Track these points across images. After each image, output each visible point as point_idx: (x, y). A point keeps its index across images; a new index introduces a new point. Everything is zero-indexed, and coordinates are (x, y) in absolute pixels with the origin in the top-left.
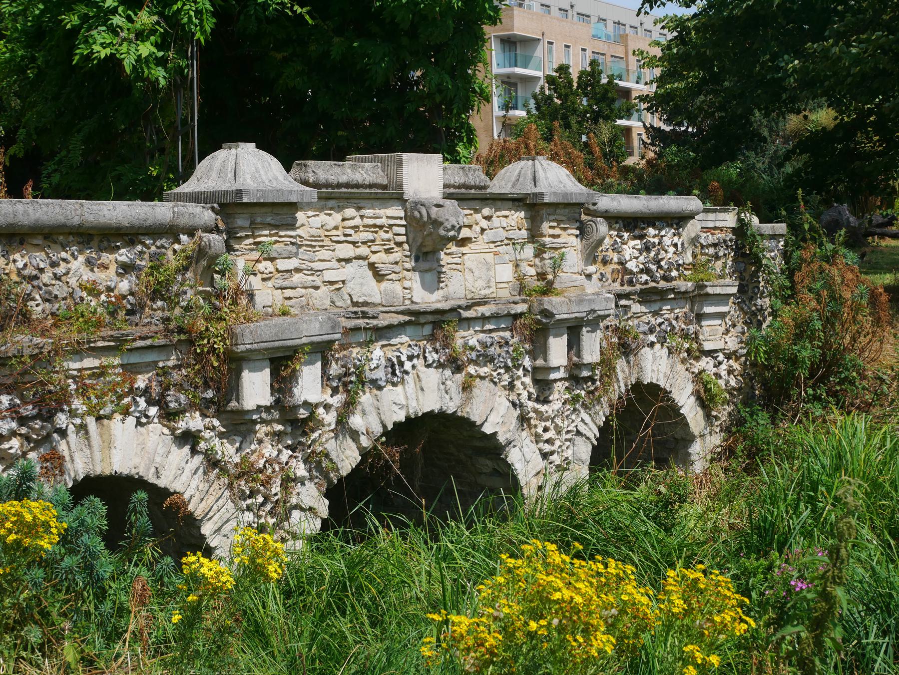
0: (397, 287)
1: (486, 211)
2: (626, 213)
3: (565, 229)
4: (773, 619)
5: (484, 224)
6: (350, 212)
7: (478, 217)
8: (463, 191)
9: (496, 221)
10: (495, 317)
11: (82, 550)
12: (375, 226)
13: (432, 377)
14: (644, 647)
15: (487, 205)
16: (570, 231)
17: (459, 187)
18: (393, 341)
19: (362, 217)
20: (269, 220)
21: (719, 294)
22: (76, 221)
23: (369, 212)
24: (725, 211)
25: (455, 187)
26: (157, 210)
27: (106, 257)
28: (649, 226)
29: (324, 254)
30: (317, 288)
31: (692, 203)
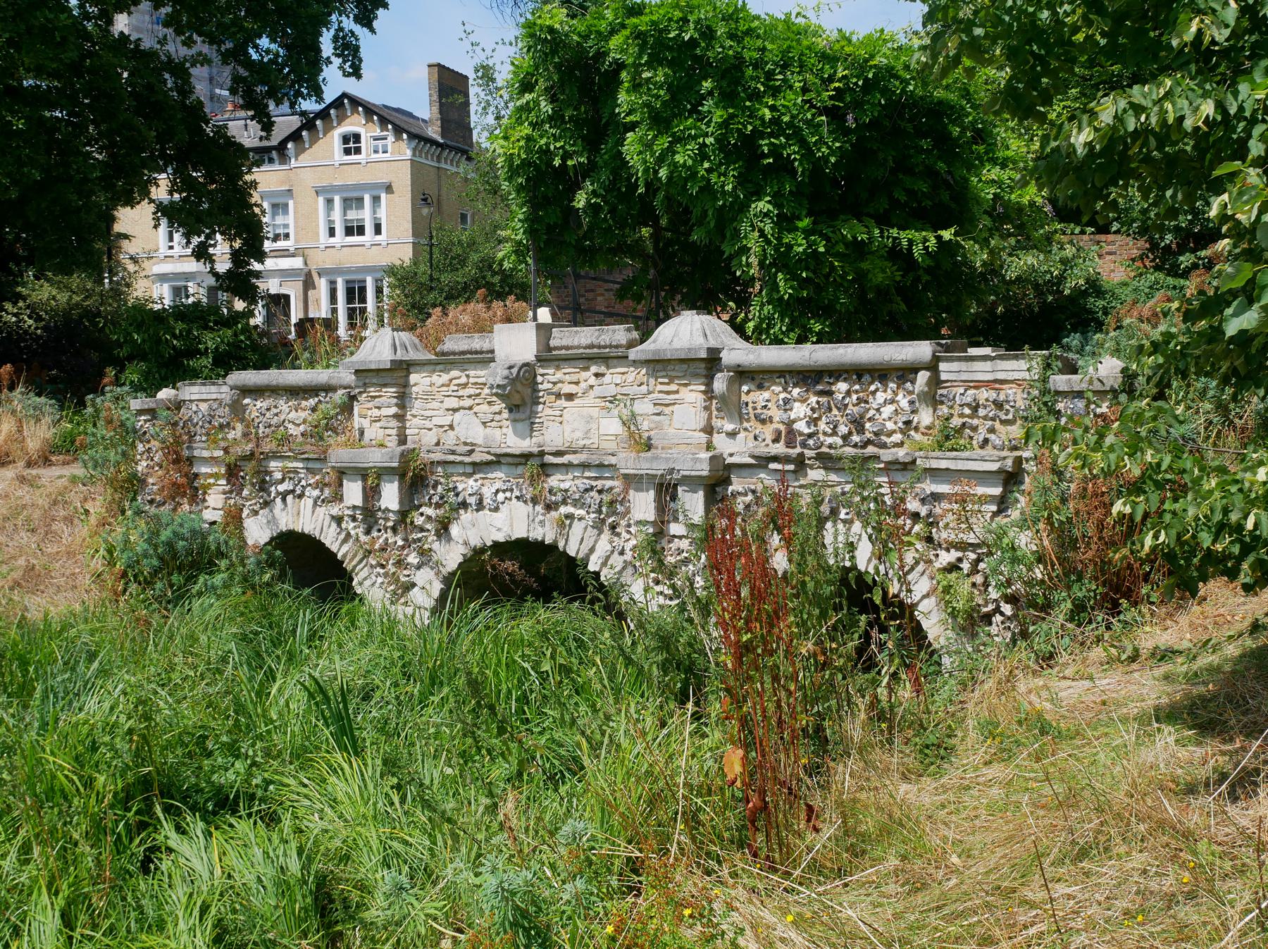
0: (498, 432)
1: (594, 369)
2: (881, 364)
3: (686, 385)
4: (18, 284)
5: (592, 380)
6: (454, 373)
7: (584, 375)
8: (595, 350)
9: (607, 379)
10: (584, 466)
11: (232, 502)
12: (996, 381)
13: (522, 510)
14: (734, 887)
15: (596, 363)
16: (691, 387)
17: (585, 348)
18: (489, 476)
19: (468, 376)
20: (374, 381)
21: (947, 469)
22: (274, 383)
23: (472, 373)
24: (1016, 358)
25: (585, 348)
26: (807, 354)
27: (304, 403)
28: (837, 380)
29: (435, 405)
30: (430, 429)
31: (921, 350)
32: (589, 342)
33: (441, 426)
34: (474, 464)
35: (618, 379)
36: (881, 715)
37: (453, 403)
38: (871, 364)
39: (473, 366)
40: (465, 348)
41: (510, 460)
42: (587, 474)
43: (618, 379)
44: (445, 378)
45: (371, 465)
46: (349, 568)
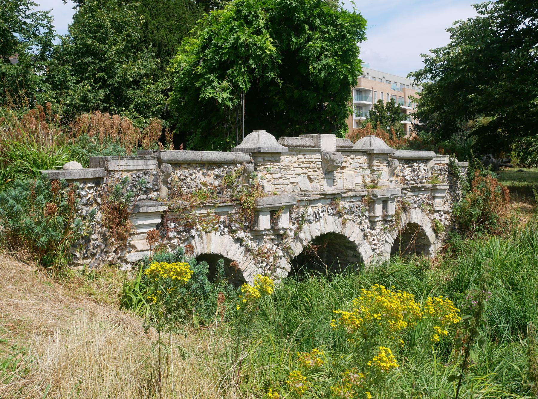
1: (352, 156)
6: (300, 156)
7: (349, 158)
8: (343, 148)
9: (355, 160)
10: (355, 196)
15: (352, 154)
17: (342, 147)
18: (316, 205)
20: (270, 159)
22: (199, 159)
23: (307, 156)
25: (340, 147)
26: (229, 155)
27: (210, 172)
30: (287, 185)
32: (343, 145)
33: (293, 183)
34: (310, 200)
35: (359, 161)
36: (350, 277)
37: (299, 171)
38: (220, 161)
39: (307, 153)
40: (298, 144)
41: (330, 197)
42: (352, 200)
43: (359, 161)
44: (295, 158)
45: (283, 204)
46: (242, 269)
